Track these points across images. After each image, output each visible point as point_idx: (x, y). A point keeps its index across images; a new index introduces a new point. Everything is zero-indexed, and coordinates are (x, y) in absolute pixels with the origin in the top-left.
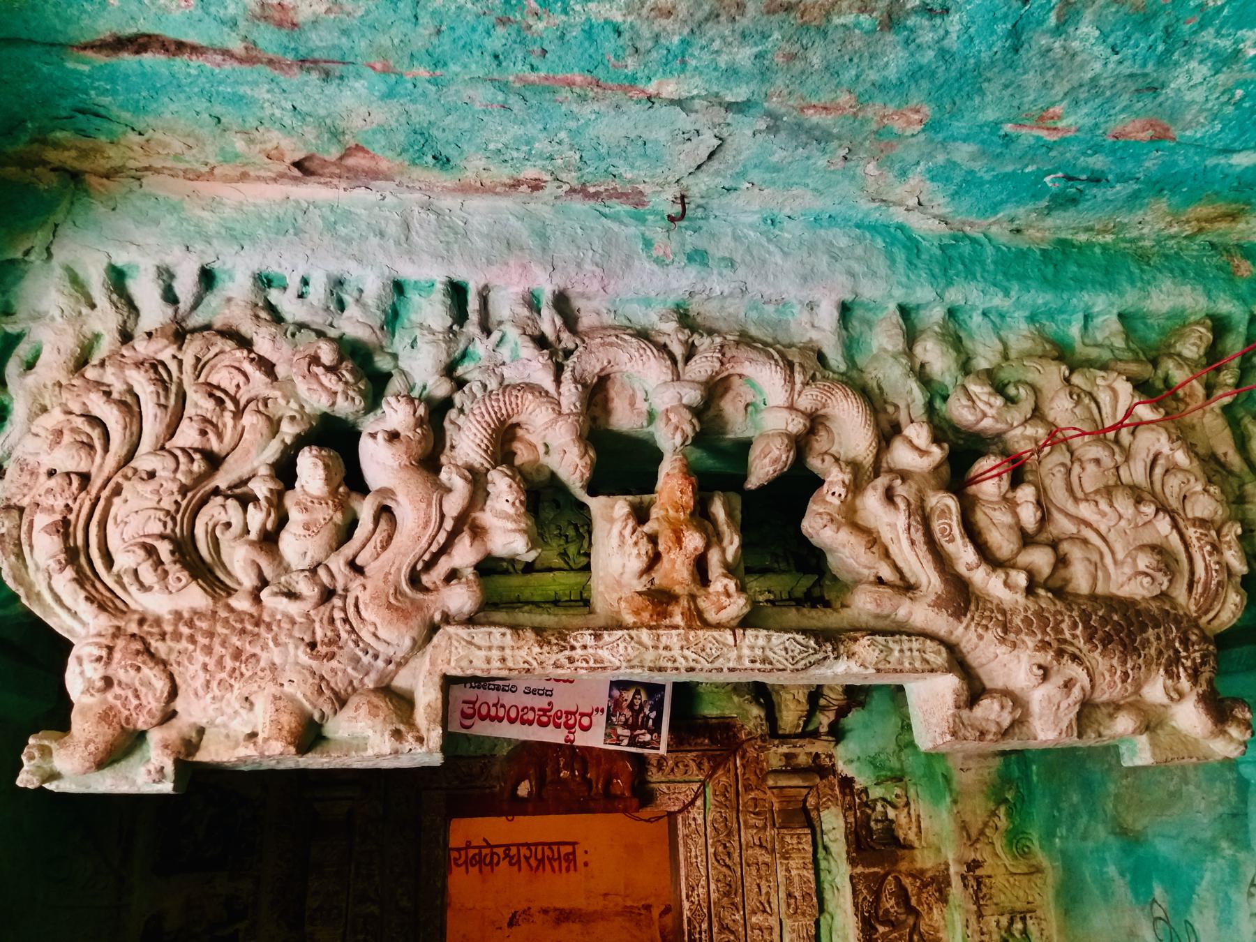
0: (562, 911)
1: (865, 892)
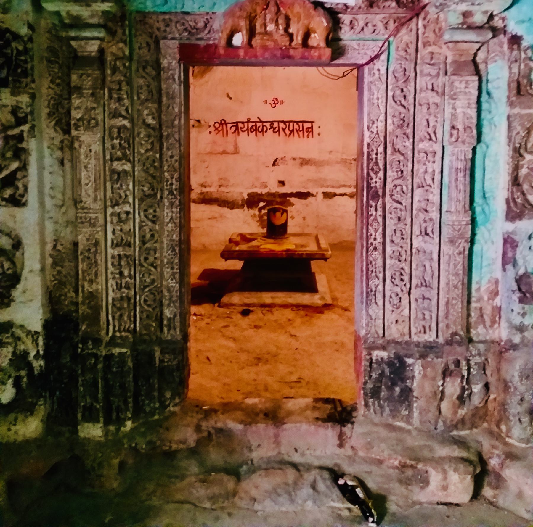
0: (304, 159)
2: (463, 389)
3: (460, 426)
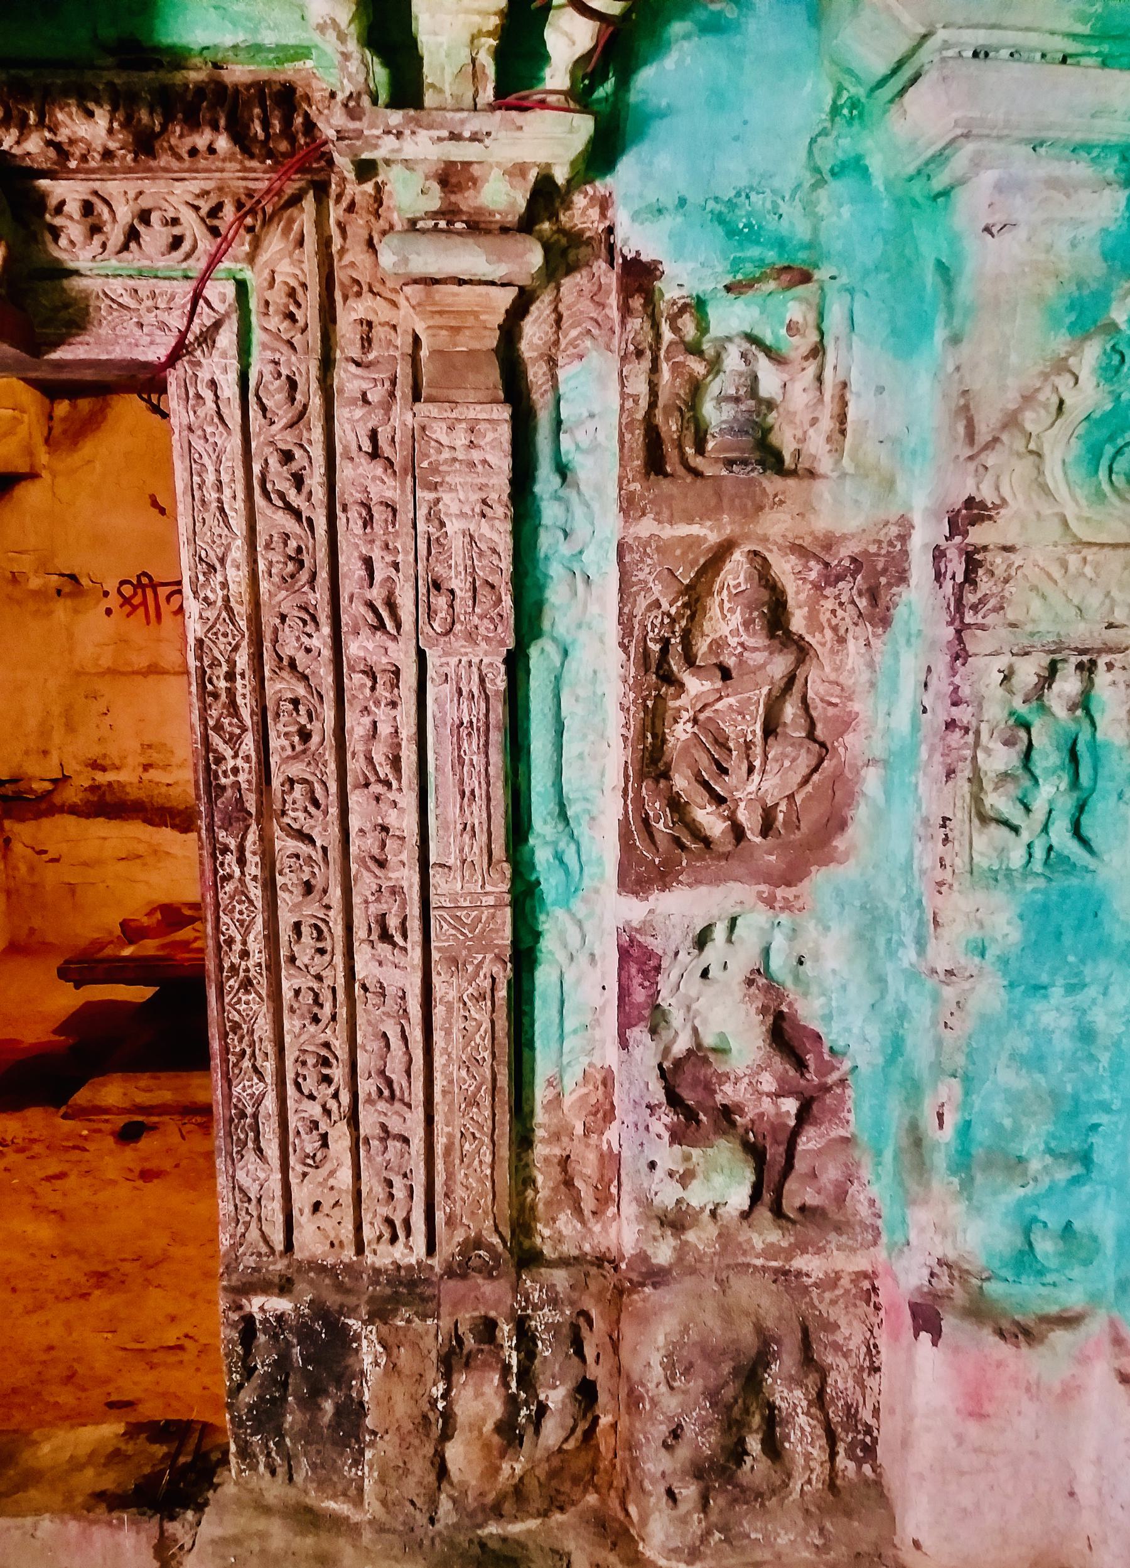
1: (657, 589)
2: (512, 1403)
3: (508, 1507)
